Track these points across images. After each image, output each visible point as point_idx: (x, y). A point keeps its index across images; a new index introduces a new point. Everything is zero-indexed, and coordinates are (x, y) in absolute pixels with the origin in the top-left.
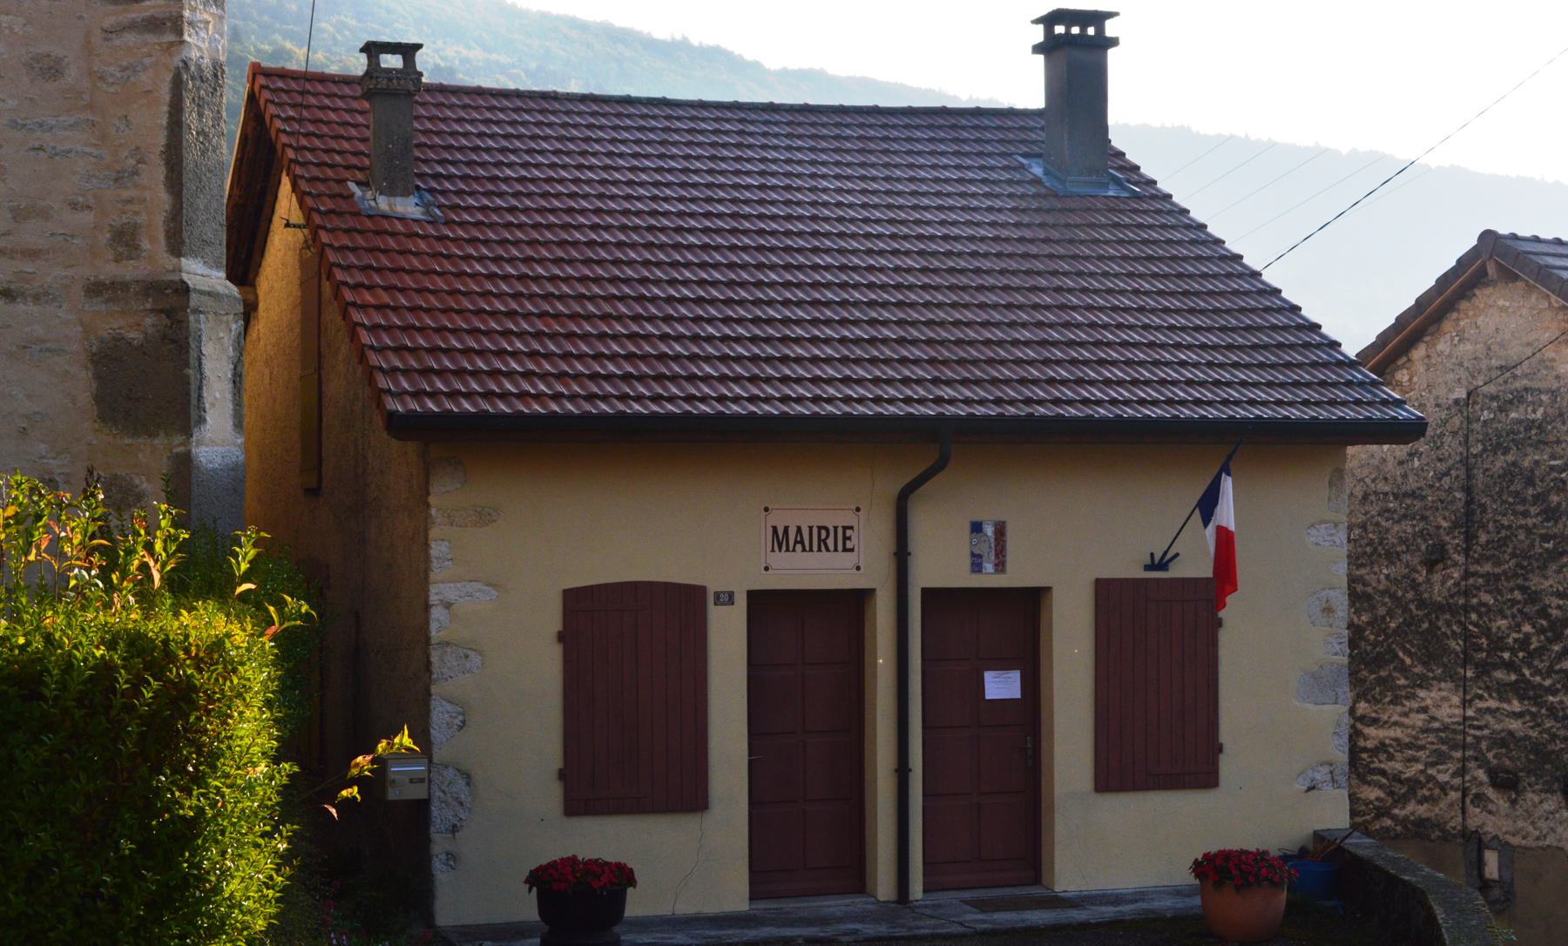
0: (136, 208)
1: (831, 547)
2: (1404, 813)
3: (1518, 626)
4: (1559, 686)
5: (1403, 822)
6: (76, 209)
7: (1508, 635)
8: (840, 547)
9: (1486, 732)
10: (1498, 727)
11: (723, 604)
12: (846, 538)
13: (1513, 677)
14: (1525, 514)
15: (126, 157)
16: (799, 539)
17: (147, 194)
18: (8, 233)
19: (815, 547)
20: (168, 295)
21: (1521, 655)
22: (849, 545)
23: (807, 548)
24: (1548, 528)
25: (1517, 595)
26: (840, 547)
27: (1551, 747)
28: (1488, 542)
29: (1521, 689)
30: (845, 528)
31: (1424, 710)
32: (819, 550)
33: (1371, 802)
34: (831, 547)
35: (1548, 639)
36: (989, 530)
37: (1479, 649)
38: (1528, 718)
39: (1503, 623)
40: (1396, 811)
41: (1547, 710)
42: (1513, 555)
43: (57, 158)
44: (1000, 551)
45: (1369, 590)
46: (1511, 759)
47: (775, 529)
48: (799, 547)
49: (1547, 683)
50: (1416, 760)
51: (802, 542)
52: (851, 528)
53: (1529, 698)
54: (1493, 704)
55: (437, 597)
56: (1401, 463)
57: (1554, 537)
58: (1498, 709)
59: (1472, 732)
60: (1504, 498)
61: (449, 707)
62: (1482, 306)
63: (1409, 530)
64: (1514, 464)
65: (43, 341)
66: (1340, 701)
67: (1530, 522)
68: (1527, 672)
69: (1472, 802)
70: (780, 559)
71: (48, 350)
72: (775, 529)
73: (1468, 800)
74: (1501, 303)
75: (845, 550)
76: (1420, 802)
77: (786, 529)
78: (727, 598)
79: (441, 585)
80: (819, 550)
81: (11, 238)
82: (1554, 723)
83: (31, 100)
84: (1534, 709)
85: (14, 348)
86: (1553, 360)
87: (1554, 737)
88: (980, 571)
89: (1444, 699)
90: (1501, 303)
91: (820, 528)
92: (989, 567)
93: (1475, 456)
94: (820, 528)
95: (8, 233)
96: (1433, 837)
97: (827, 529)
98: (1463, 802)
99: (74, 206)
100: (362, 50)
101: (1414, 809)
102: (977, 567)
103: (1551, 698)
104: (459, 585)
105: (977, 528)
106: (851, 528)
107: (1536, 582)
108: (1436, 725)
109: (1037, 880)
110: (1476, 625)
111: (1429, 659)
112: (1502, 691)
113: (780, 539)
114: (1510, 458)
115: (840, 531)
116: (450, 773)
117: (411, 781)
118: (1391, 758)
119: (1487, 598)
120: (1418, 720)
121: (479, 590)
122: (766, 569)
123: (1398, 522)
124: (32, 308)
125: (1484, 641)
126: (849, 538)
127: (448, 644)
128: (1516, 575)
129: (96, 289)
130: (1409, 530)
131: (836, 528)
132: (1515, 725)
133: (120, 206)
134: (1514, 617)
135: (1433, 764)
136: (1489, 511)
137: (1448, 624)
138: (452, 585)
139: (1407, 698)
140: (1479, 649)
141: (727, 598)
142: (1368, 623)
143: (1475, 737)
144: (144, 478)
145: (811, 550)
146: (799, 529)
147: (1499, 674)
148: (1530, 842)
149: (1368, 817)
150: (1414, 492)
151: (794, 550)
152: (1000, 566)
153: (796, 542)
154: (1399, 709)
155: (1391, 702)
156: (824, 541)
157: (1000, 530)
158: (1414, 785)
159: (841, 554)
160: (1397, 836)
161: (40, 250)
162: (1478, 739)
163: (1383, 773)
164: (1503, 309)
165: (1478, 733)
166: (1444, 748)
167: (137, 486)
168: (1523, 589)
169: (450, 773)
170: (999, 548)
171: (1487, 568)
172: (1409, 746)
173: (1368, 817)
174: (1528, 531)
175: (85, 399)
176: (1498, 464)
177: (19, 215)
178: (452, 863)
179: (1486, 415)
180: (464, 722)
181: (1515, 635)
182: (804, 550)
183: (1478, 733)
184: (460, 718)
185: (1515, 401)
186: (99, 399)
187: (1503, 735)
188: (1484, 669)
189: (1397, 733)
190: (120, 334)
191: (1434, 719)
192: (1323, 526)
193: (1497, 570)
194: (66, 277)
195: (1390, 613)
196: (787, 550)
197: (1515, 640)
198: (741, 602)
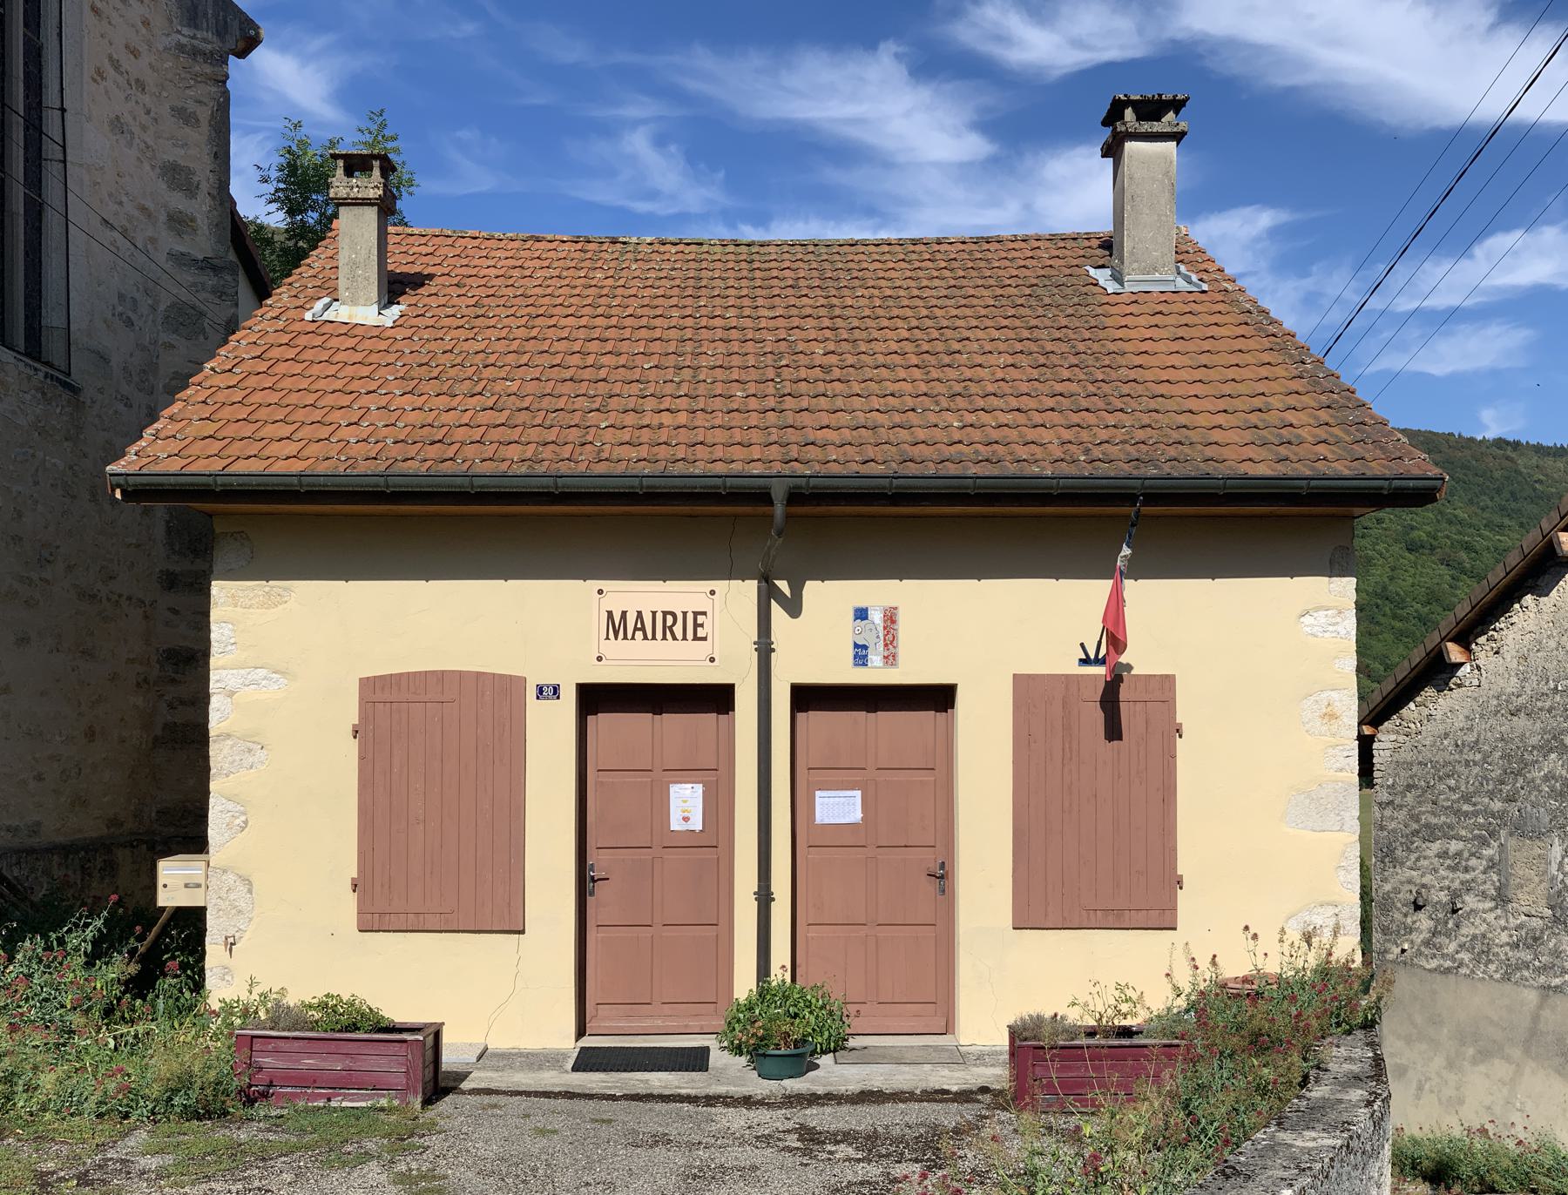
12: (696, 625)
19: (659, 634)
30: (696, 614)
47: (610, 614)
51: (643, 629)
52: (704, 613)
70: (617, 648)
72: (610, 614)
75: (696, 638)
79: (224, 672)
91: (665, 614)
104: (242, 672)
113: (616, 626)
115: (690, 617)
138: (235, 671)
159: (690, 642)
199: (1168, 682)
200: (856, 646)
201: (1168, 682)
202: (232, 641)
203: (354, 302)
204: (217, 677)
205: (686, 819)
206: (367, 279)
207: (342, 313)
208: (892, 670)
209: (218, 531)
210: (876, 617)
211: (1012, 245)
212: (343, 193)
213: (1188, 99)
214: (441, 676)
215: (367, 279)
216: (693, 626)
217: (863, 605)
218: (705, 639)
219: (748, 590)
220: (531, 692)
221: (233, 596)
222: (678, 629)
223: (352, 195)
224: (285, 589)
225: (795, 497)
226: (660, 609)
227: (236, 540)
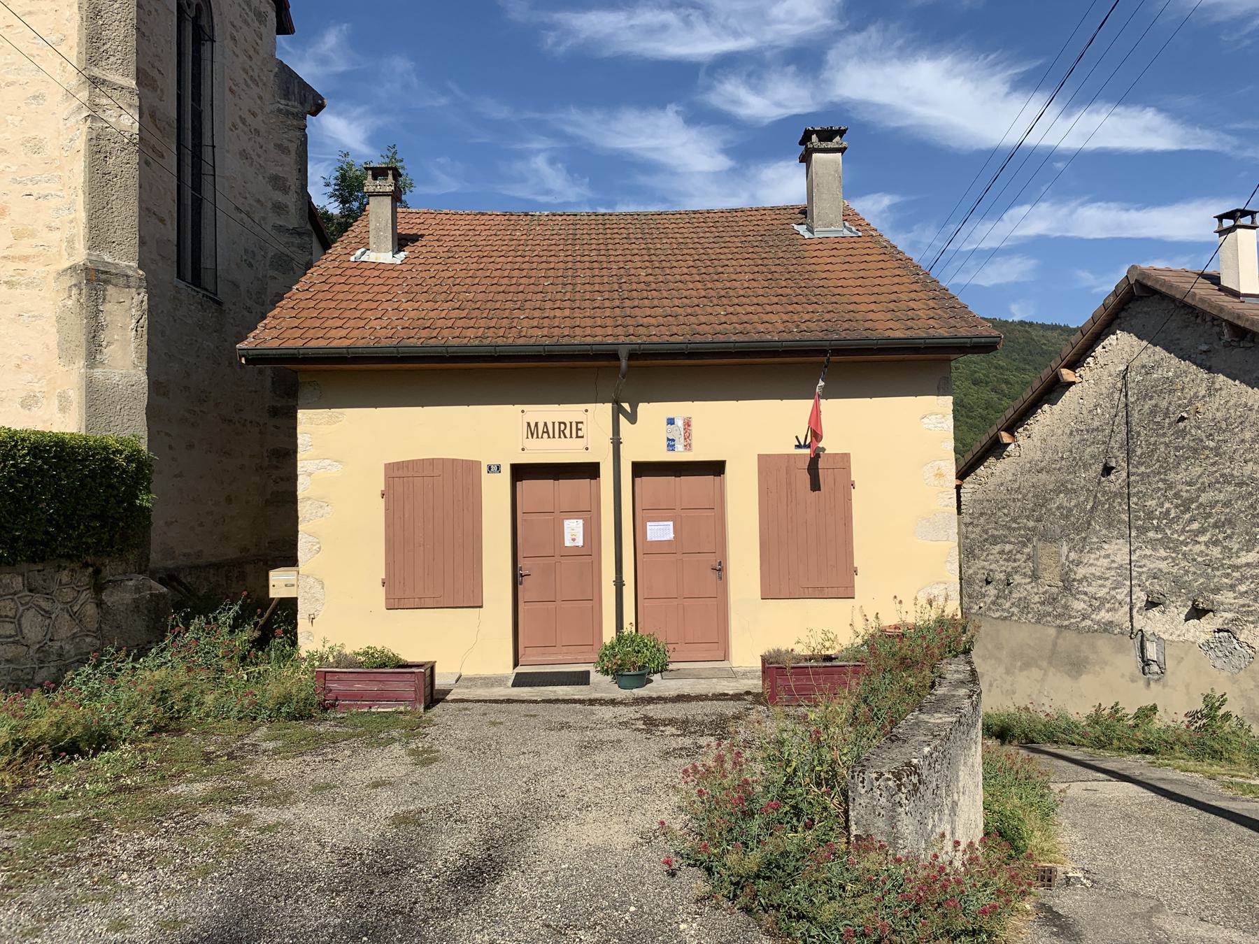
1: (568, 435)
2: (1098, 617)
3: (1162, 505)
4: (1188, 540)
5: (1098, 623)
7: (1156, 510)
9: (1145, 569)
10: (1152, 566)
11: (493, 472)
12: (578, 429)
13: (1160, 536)
14: (1164, 435)
16: (545, 430)
18: (11, 247)
19: (557, 435)
21: (1164, 521)
22: (580, 434)
23: (551, 436)
24: (1179, 442)
25: (1161, 485)
27: (1186, 578)
28: (1142, 454)
29: (1166, 542)
30: (577, 423)
31: (1107, 556)
32: (560, 437)
33: (1080, 611)
34: (568, 435)
35: (1181, 511)
36: (679, 423)
37: (1139, 518)
38: (1170, 560)
39: (1154, 503)
40: (1093, 616)
41: (1182, 555)
42: (1158, 461)
44: (687, 437)
45: (1075, 487)
46: (1161, 586)
48: (545, 435)
49: (1182, 538)
50: (1104, 586)
51: (548, 432)
52: (582, 423)
53: (1170, 548)
54: (1148, 552)
56: (1090, 411)
57: (1183, 448)
58: (1151, 555)
59: (1136, 569)
60: (1151, 426)
61: (311, 539)
62: (1134, 313)
63: (1096, 450)
64: (1156, 406)
66: (950, 538)
67: (1167, 440)
68: (1169, 532)
69: (1138, 612)
70: (533, 443)
71: (34, 316)
73: (1135, 611)
74: (1145, 309)
75: (577, 437)
76: (1108, 611)
77: (536, 424)
78: (495, 469)
79: (306, 462)
80: (560, 437)
81: (12, 249)
82: (1187, 563)
83: (25, 165)
84: (1174, 555)
85: (13, 317)
86: (1179, 339)
87: (1187, 572)
88: (673, 450)
89: (1120, 549)
90: (1145, 309)
91: (560, 423)
92: (679, 447)
93: (1132, 403)
94: (560, 423)
95: (11, 247)
96: (1116, 632)
97: (565, 424)
98: (1131, 613)
99: (50, 228)
101: (1104, 616)
102: (671, 444)
103: (1184, 548)
104: (316, 461)
106: (582, 423)
107: (1171, 476)
108: (1114, 565)
109: (726, 657)
110: (1136, 504)
111: (1110, 525)
112: (1153, 543)
113: (532, 430)
114: (1153, 402)
115: (574, 425)
116: (311, 580)
117: (286, 586)
118: (1089, 585)
119: (1143, 488)
120: (1105, 562)
122: (523, 450)
124: (24, 291)
125: (1142, 514)
126: (580, 429)
127: (309, 499)
128: (1159, 473)
130: (1096, 450)
131: (571, 423)
132: (1163, 565)
134: (1159, 499)
135: (1115, 589)
136: (1142, 434)
137: (1120, 504)
139: (1098, 549)
140: (1139, 518)
141: (495, 469)
142: (1075, 506)
143: (1138, 572)
145: (554, 437)
146: (545, 424)
147: (1151, 534)
148: (1174, 638)
149: (1078, 620)
150: (1098, 428)
151: (542, 437)
152: (688, 447)
153: (544, 432)
154: (1093, 556)
155: (1088, 552)
156: (563, 432)
157: (687, 424)
158: (1103, 601)
160: (1096, 631)
161: (30, 256)
162: (1140, 574)
163: (1086, 594)
164: (1146, 313)
165: (1140, 570)
166: (1119, 579)
168: (1164, 481)
169: (311, 580)
170: (687, 434)
171: (1142, 469)
172: (1100, 578)
173: (1078, 620)
174: (1167, 445)
175: (53, 345)
176: (1147, 407)
177: (19, 235)
178: (311, 638)
179: (1139, 378)
180: (320, 548)
181: (1159, 509)
182: (549, 437)
183: (1140, 570)
184: (318, 546)
185: (1156, 367)
187: (1155, 571)
188: (1143, 530)
189: (1093, 570)
191: (1113, 561)
192: (934, 417)
193: (1148, 471)
195: (1087, 500)
196: (538, 437)
197: (1161, 513)
198: (506, 473)
201: (846, 457)
203: (378, 250)
205: (574, 540)
207: (371, 257)
212: (371, 189)
216: (576, 430)
219: (601, 412)
220: (484, 469)
223: (377, 190)
224: (341, 414)
225: (633, 356)
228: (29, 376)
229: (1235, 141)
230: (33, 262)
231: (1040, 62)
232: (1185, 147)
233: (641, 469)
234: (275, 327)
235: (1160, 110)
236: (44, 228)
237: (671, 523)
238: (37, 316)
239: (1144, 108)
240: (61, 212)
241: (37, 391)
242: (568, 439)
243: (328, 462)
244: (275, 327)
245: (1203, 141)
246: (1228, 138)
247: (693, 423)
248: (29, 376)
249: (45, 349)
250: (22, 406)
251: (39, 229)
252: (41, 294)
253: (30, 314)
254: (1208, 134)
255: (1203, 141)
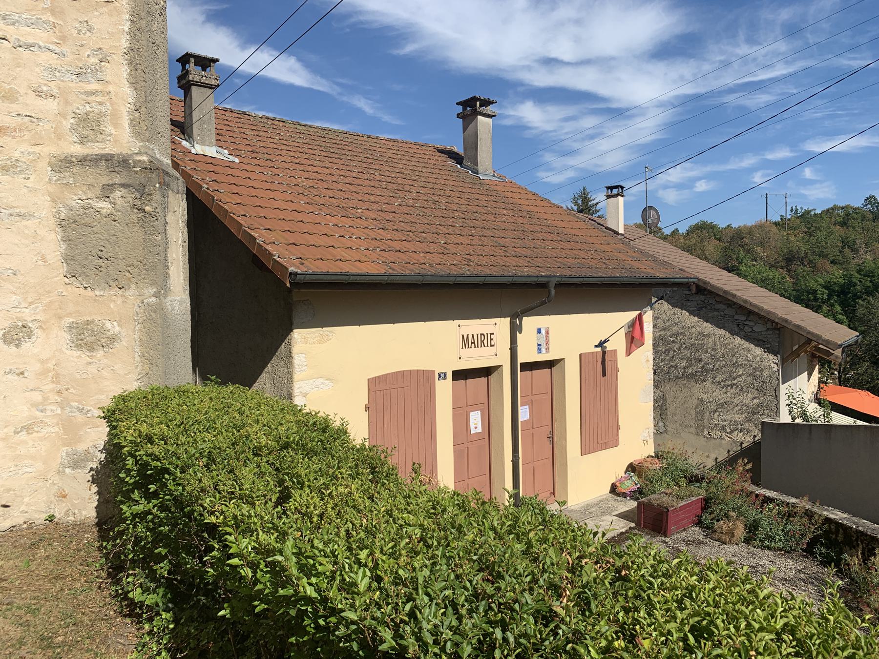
0: (99, 99)
6: (40, 96)
8: (489, 345)
12: (492, 339)
15: (89, 56)
17: (111, 88)
19: (479, 345)
20: (136, 173)
26: (489, 345)
30: (491, 334)
43: (20, 49)
47: (463, 336)
48: (473, 345)
51: (474, 343)
52: (493, 334)
55: (299, 390)
65: (13, 207)
70: (466, 352)
71: (18, 215)
72: (463, 336)
75: (491, 346)
78: (442, 376)
79: (301, 383)
91: (481, 334)
92: (543, 350)
97: (483, 335)
99: (38, 93)
100: (177, 61)
102: (539, 351)
104: (311, 381)
105: (539, 331)
106: (493, 334)
113: (467, 342)
115: (489, 335)
121: (323, 384)
122: (460, 358)
123: (30, 328)
129: (64, 164)
133: (84, 97)
138: (307, 382)
141: (442, 376)
144: (115, 323)
159: (489, 348)
167: (109, 331)
186: (67, 259)
190: (89, 204)
194: (33, 153)
198: (450, 376)
199: (615, 351)
200: (538, 345)
201: (615, 351)
202: (305, 364)
203: (203, 143)
204: (298, 386)
205: (476, 428)
206: (210, 131)
207: (198, 149)
208: (548, 355)
209: (295, 299)
210: (543, 332)
211: (261, 120)
212: (197, 79)
213: (457, 104)
214: (403, 373)
215: (210, 131)
216: (485, 340)
217: (539, 327)
218: (493, 346)
219: (504, 323)
220: (437, 377)
221: (305, 338)
222: (485, 342)
223: (202, 81)
224: (330, 332)
225: (559, 285)
226: (479, 333)
227: (305, 304)
228: (14, 299)
229: (338, 89)
230: (13, 137)
231: (225, 6)
232: (312, 87)
233: (528, 367)
234: (274, 243)
235: (299, 60)
236: (30, 91)
237: (527, 407)
238: (24, 215)
239: (290, 56)
240: (57, 74)
241: (29, 319)
242: (486, 348)
243: (321, 380)
244: (274, 243)
245: (321, 85)
246: (335, 87)
247: (550, 332)
248: (14, 299)
249: (40, 262)
250: (5, 341)
251: (22, 91)
252: (29, 183)
253: (11, 211)
254: (324, 81)
255: (321, 85)
